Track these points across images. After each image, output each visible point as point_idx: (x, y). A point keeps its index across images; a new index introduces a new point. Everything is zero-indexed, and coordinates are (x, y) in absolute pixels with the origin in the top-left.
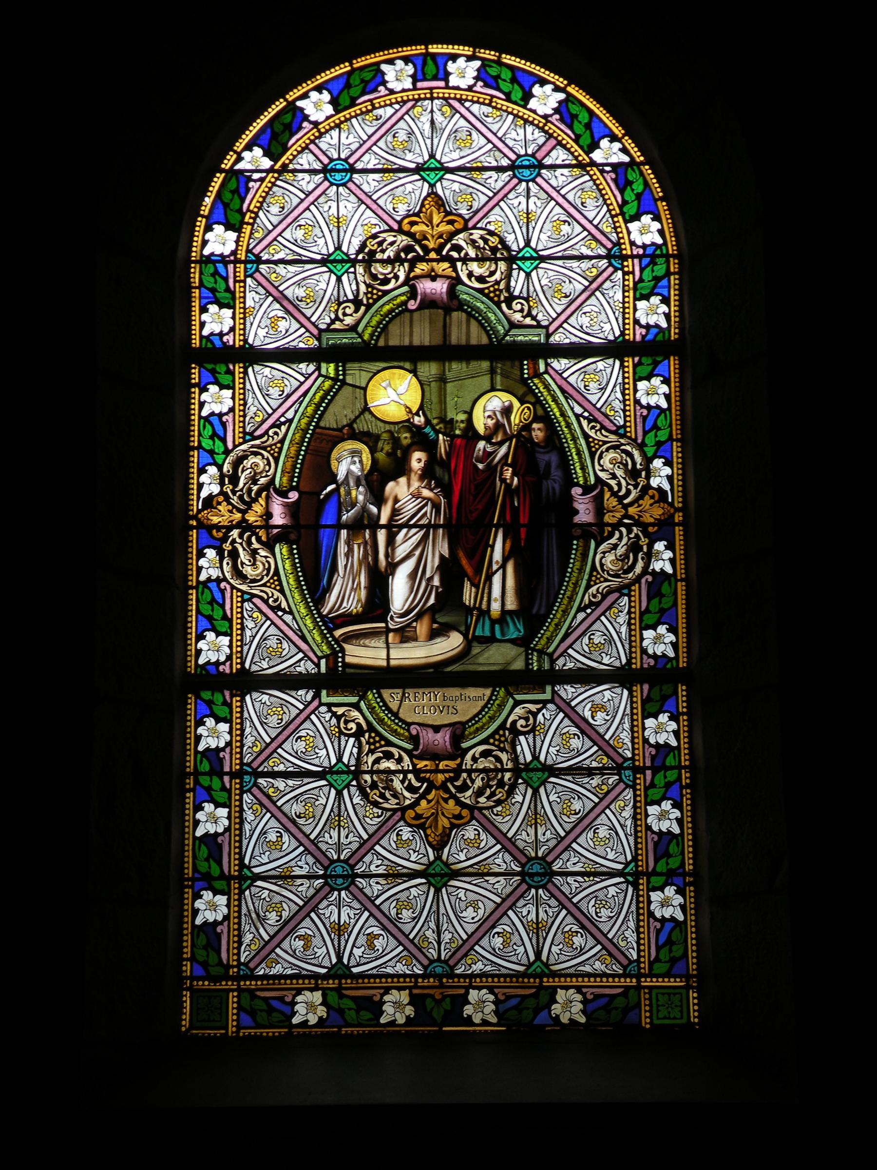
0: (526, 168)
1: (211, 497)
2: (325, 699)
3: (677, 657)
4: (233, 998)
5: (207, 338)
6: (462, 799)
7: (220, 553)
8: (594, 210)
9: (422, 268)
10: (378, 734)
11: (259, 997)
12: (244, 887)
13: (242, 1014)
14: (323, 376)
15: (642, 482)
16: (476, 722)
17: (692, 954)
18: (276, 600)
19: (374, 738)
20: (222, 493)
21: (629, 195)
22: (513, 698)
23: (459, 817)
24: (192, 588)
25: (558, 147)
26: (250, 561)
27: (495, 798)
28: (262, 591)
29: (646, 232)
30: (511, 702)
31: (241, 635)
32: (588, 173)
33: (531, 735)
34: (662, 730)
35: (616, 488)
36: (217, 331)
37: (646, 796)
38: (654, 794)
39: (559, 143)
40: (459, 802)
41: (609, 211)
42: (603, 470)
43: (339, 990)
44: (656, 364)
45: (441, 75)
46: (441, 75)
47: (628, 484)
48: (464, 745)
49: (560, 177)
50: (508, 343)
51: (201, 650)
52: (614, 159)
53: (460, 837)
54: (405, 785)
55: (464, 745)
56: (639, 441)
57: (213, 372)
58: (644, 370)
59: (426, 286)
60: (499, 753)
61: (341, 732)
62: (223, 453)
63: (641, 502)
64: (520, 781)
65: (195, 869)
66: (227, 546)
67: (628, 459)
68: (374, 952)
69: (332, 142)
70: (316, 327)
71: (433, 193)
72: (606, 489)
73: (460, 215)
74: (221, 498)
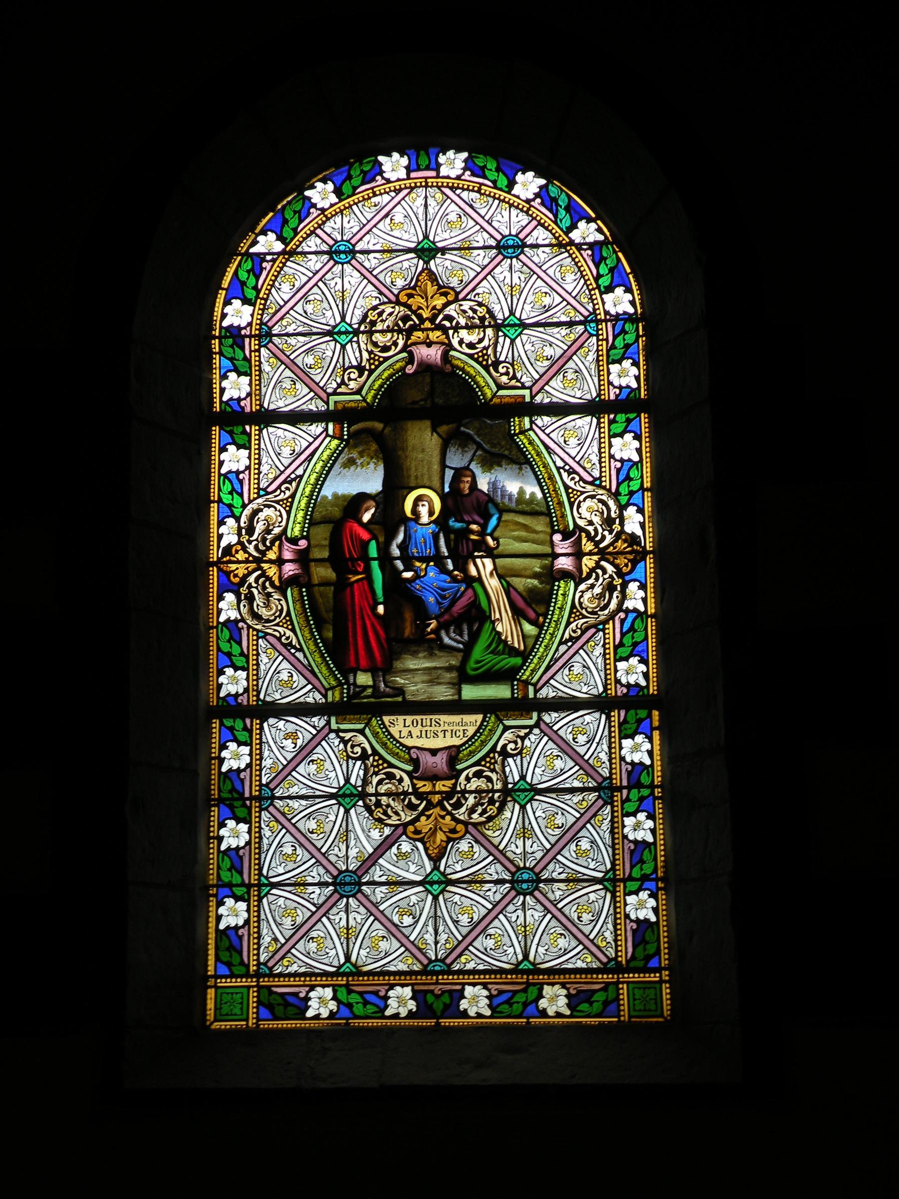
0: (509, 248)
1: (229, 547)
2: (526, 392)
3: (647, 687)
4: (253, 993)
5: (227, 403)
6: (457, 816)
7: (238, 595)
8: (571, 282)
9: (418, 335)
10: (381, 757)
11: (276, 993)
12: (262, 895)
13: (261, 1008)
14: (330, 436)
15: (617, 527)
16: (470, 746)
17: (664, 952)
18: (288, 638)
19: (484, 360)
20: (240, 543)
21: (603, 269)
22: (503, 724)
23: (453, 831)
24: (212, 628)
25: (539, 227)
26: (264, 603)
27: (485, 816)
28: (275, 630)
29: (620, 302)
30: (501, 727)
31: (257, 670)
32: (568, 251)
33: (519, 757)
34: (638, 750)
35: (267, 584)
36: (236, 397)
37: (622, 809)
38: (630, 807)
39: (540, 224)
40: (454, 819)
41: (585, 283)
42: (581, 518)
43: (347, 986)
44: (629, 421)
45: (433, 165)
46: (433, 165)
47: (604, 530)
48: (459, 767)
49: (541, 255)
50: (495, 404)
51: (225, 389)
52: (590, 239)
53: (454, 850)
54: (406, 803)
55: (459, 767)
56: (613, 490)
57: (231, 433)
58: (618, 428)
59: (422, 352)
60: (489, 774)
61: (348, 757)
62: (242, 507)
63: (246, 572)
64: (509, 799)
65: (219, 877)
66: (244, 590)
67: (604, 508)
68: (377, 951)
69: (336, 227)
70: (325, 391)
71: (427, 268)
72: (583, 535)
73: (453, 289)
74: (239, 547)
